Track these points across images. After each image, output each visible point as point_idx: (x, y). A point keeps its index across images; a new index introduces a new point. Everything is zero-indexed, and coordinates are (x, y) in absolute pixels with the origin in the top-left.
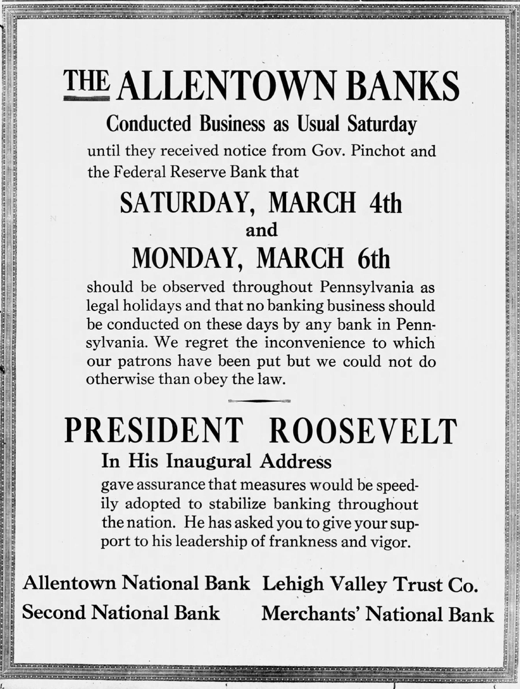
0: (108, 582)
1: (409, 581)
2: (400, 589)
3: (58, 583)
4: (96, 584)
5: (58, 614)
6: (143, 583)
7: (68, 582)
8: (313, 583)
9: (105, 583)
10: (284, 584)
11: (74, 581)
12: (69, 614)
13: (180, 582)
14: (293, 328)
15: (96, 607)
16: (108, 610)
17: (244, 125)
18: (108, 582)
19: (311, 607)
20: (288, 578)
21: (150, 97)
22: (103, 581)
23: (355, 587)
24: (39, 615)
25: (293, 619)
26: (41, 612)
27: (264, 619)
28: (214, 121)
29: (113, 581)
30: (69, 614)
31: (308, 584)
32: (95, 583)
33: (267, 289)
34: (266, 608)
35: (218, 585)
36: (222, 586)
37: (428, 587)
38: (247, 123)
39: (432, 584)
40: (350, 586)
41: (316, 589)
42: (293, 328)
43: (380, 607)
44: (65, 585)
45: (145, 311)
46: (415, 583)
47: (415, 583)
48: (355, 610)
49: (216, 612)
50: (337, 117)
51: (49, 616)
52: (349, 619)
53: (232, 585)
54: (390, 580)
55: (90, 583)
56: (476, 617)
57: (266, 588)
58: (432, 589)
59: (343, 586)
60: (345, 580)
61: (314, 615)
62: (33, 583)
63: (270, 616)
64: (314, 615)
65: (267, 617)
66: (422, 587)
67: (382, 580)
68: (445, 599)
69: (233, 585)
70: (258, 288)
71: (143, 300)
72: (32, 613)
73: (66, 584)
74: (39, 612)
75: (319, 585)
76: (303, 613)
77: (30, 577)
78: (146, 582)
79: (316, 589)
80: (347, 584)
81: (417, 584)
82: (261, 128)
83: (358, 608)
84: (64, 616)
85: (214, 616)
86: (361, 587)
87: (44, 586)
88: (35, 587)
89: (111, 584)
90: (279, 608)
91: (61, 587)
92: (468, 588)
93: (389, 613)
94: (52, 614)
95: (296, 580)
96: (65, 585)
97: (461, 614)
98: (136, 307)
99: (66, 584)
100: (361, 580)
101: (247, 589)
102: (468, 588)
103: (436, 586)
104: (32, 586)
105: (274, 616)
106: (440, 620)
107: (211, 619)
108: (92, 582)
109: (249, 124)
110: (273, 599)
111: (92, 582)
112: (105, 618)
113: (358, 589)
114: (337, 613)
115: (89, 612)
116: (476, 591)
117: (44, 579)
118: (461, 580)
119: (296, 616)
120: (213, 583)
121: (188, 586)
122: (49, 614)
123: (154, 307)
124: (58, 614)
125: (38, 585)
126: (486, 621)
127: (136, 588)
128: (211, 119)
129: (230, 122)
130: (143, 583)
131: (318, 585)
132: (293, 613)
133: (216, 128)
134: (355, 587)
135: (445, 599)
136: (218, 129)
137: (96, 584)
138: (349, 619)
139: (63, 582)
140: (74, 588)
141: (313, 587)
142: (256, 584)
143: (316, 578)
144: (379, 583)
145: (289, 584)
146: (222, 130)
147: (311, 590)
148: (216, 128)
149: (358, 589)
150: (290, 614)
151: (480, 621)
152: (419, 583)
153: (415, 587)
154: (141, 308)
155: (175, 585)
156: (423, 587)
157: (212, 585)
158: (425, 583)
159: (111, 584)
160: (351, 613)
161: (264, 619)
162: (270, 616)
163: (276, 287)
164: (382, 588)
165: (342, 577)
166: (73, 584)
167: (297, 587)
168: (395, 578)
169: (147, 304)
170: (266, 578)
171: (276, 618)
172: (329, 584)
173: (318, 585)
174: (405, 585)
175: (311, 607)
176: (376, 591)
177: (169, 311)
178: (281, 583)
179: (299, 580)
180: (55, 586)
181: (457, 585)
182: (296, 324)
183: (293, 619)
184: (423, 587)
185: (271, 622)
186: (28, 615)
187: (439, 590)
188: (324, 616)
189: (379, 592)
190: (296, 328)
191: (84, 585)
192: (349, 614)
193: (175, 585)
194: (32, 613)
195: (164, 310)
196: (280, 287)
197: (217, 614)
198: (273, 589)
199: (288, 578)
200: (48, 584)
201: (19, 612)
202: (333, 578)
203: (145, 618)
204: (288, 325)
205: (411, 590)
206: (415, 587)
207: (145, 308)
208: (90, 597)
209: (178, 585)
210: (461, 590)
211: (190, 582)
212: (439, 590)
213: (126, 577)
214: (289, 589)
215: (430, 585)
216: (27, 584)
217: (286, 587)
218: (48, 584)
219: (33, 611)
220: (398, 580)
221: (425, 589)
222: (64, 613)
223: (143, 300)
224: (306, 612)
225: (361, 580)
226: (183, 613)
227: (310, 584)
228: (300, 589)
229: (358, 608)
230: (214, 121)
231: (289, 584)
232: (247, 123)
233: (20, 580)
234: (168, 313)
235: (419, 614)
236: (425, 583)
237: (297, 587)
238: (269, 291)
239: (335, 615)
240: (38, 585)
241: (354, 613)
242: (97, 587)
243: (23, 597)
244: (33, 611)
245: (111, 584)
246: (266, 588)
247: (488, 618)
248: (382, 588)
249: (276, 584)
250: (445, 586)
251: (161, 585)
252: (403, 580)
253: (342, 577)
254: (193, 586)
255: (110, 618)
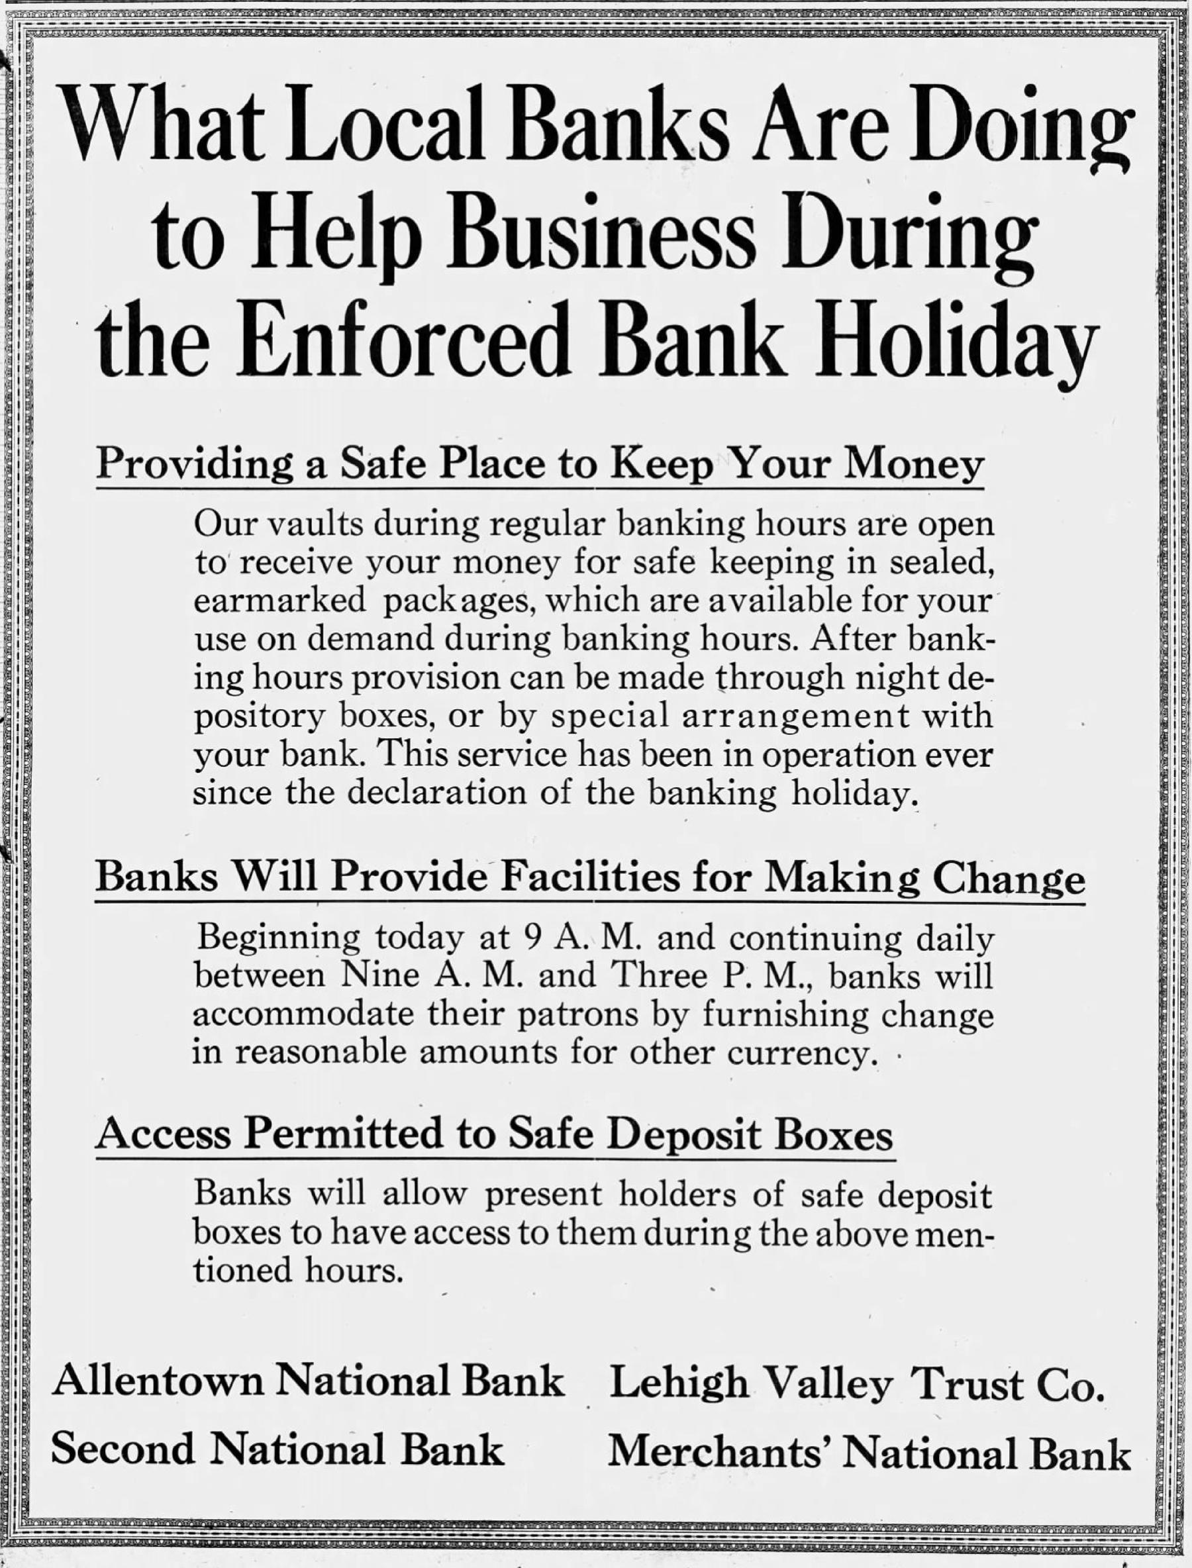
0: (246, 1378)
1: (948, 1377)
2: (928, 1395)
3: (132, 1381)
4: (220, 1384)
5: (133, 1453)
6: (324, 1379)
7: (154, 1377)
8: (725, 1381)
9: (240, 1382)
10: (658, 1383)
11: (169, 1376)
12: (158, 1452)
13: (408, 1378)
14: (520, 723)
15: (220, 1436)
16: (248, 1444)
17: (656, 238)
18: (246, 1378)
19: (720, 1438)
20: (668, 1368)
21: (308, 153)
22: (234, 1377)
23: (820, 1390)
24: (88, 1456)
25: (679, 1463)
26: (94, 1449)
27: (614, 1463)
28: (512, 224)
29: (258, 1377)
30: (158, 1452)
31: (712, 1383)
32: (216, 1381)
33: (795, 683)
34: (617, 1438)
35: (493, 1386)
36: (500, 1386)
37: (990, 1390)
38: (669, 230)
39: (1000, 1384)
40: (808, 1389)
41: (731, 1394)
42: (520, 723)
43: (875, 1437)
44: (149, 1384)
45: (842, 807)
46: (961, 1381)
47: (961, 1381)
48: (821, 1444)
49: (496, 1447)
50: (476, 92)
51: (112, 1458)
52: (807, 1464)
53: (524, 1385)
54: (901, 1374)
55: (205, 1381)
56: (1092, 1459)
57: (618, 1393)
58: (999, 1395)
59: (793, 1389)
60: (797, 1376)
61: (727, 1455)
62: (75, 1381)
63: (627, 1458)
64: (727, 1455)
65: (620, 1458)
66: (978, 1391)
67: (882, 1375)
68: (1027, 1418)
69: (527, 1384)
70: (775, 680)
71: (836, 780)
72: (71, 1451)
73: (150, 1383)
74: (88, 1447)
75: (738, 1386)
76: (702, 1452)
77: (69, 1367)
78: (329, 1377)
79: (731, 1394)
80: (801, 1383)
81: (966, 1384)
82: (740, 256)
83: (827, 1439)
84: (146, 1457)
85: (491, 1457)
86: (833, 1390)
87: (101, 1387)
88: (80, 1391)
89: (253, 1383)
90: (647, 1439)
91: (138, 1390)
92: (1083, 1391)
93: (896, 1450)
94: (118, 1453)
95: (687, 1375)
96: (149, 1384)
97: (489, 1378)
98: (822, 796)
99: (150, 1383)
100: (834, 1375)
101: (558, 1393)
102: (1083, 1391)
103: (1009, 1387)
104: (73, 1388)
105: (635, 1458)
106: (1012, 1466)
107: (485, 1462)
108: (209, 1378)
109: (682, 235)
110: (633, 1416)
111: (209, 1378)
112: (242, 1462)
113: (827, 1395)
114: (780, 1450)
115: (204, 1447)
116: (1101, 1398)
117: (101, 1372)
118: (1065, 1373)
119: (687, 1457)
120: (483, 1381)
121: (427, 1386)
122: (111, 1453)
123: (861, 797)
124: (133, 1453)
125: (87, 1386)
126: (1114, 1467)
127: (307, 1392)
128: (501, 212)
129: (591, 225)
130: (324, 1379)
131: (737, 1386)
132: (679, 1450)
133: (524, 253)
134: (820, 1390)
135: (1027, 1418)
136: (535, 260)
137: (220, 1384)
138: (807, 1464)
139: (143, 1379)
140: (169, 1391)
141: (724, 1389)
142: (586, 1382)
143: (731, 1369)
144: (876, 1381)
145: (671, 1383)
146: (553, 263)
147: (720, 1397)
148: (524, 253)
149: (827, 1395)
150: (674, 1452)
151: (1101, 1467)
152: (971, 1382)
153: (961, 1391)
154: (833, 799)
155: (396, 1384)
156: (980, 1391)
157: (478, 1386)
158: (984, 1382)
159: (252, 1384)
160: (813, 1451)
161: (614, 1463)
162: (627, 1458)
163: (815, 678)
164: (882, 1393)
165: (792, 1368)
166: (168, 1383)
167: (688, 1389)
168: (915, 1370)
169: (847, 790)
170: (618, 1368)
171: (642, 1462)
172: (760, 1384)
173: (737, 1386)
174: (939, 1385)
175: (720, 1438)
176: (868, 1398)
177: (897, 804)
178: (651, 1381)
179: (693, 1374)
180: (125, 1388)
181: (1056, 1384)
182: (528, 715)
183: (679, 1463)
184: (980, 1391)
185: (629, 1470)
186: (63, 1455)
187: (1016, 1397)
188: (750, 1458)
189: (875, 1401)
190: (527, 723)
191: (191, 1385)
192: (808, 1453)
193: (396, 1384)
194: (71, 1451)
195: (886, 803)
196: (825, 677)
197: (497, 1452)
198: (635, 1394)
199: (668, 1368)
200: (112, 1383)
201: (41, 1447)
202: (771, 1370)
203: (331, 1461)
204: (509, 718)
205: (952, 1396)
206: (961, 1391)
207: (842, 799)
208: (204, 1414)
209: (403, 1384)
210: (1066, 1396)
211: (431, 1378)
212: (1016, 1397)
213: (285, 1367)
214: (669, 1394)
215: (994, 1385)
216: (61, 1383)
217: (664, 1391)
218: (112, 1383)
219: (76, 1446)
220: (922, 1373)
221: (984, 1396)
222: (147, 1451)
223: (836, 780)
224: (708, 1450)
225: (834, 1375)
226: (528, 1234)
227: (718, 1384)
228: (695, 1394)
229: (827, 1439)
230: (512, 224)
231: (671, 1383)
232: (669, 230)
233: (44, 1372)
234: (895, 809)
235: (964, 1452)
236: (984, 1382)
237: (688, 1389)
238: (800, 686)
239: (775, 1456)
240: (87, 1386)
241: (817, 1449)
242: (221, 1390)
243: (51, 1412)
244: (76, 1446)
245: (252, 1384)
246: (618, 1393)
247: (1119, 1462)
248: (882, 1393)
249: (640, 1384)
250: (1028, 1388)
251: (364, 1386)
252: (934, 1373)
253: (792, 1368)
254: (438, 1387)
255: (253, 1461)
